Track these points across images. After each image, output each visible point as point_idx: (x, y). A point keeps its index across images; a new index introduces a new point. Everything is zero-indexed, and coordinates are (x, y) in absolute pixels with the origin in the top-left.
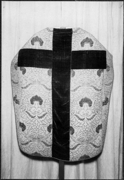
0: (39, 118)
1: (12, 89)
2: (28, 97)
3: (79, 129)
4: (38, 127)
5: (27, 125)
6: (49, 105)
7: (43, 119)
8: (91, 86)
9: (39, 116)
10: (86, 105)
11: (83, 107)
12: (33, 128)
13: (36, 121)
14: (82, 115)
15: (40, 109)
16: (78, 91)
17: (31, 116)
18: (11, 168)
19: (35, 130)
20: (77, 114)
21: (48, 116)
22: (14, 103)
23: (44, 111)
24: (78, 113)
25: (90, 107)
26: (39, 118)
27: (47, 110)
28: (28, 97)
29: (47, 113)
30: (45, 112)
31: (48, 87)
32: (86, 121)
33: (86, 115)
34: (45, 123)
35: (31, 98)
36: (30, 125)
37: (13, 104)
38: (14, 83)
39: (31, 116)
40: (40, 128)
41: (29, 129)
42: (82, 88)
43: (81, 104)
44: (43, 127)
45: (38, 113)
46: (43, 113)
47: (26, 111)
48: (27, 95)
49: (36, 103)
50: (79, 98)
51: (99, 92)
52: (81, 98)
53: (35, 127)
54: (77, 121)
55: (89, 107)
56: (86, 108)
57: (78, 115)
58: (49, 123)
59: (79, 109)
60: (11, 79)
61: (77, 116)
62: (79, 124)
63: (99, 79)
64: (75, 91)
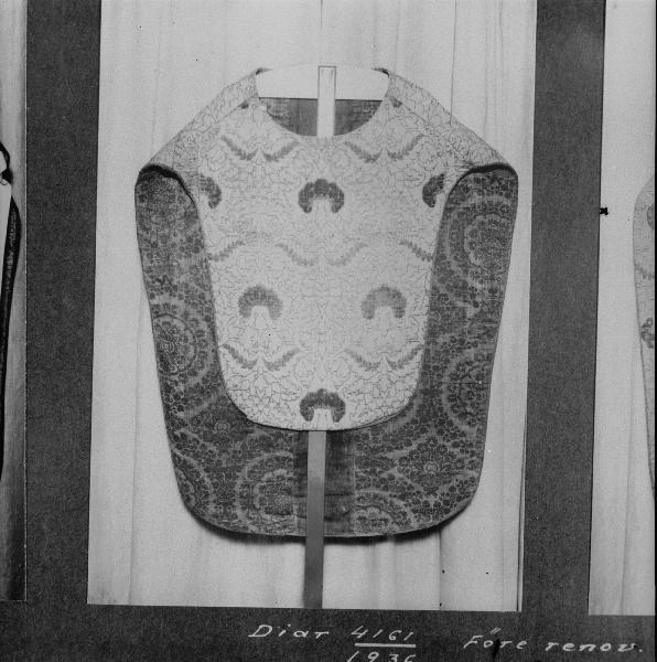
0: (271, 366)
1: (637, 296)
3: (362, 403)
5: (352, 397)
7: (283, 371)
8: (402, 243)
9: (268, 360)
10: (384, 312)
11: (374, 322)
17: (241, 360)
18: (624, 576)
22: (641, 347)
24: (359, 344)
26: (271, 366)
30: (290, 348)
31: (424, 247)
34: (292, 389)
35: (240, 294)
36: (361, 396)
37: (639, 350)
39: (241, 360)
44: (283, 402)
49: (260, 310)
51: (308, 269)
55: (395, 321)
57: (361, 352)
60: (634, 261)
62: (361, 382)
64: (344, 264)
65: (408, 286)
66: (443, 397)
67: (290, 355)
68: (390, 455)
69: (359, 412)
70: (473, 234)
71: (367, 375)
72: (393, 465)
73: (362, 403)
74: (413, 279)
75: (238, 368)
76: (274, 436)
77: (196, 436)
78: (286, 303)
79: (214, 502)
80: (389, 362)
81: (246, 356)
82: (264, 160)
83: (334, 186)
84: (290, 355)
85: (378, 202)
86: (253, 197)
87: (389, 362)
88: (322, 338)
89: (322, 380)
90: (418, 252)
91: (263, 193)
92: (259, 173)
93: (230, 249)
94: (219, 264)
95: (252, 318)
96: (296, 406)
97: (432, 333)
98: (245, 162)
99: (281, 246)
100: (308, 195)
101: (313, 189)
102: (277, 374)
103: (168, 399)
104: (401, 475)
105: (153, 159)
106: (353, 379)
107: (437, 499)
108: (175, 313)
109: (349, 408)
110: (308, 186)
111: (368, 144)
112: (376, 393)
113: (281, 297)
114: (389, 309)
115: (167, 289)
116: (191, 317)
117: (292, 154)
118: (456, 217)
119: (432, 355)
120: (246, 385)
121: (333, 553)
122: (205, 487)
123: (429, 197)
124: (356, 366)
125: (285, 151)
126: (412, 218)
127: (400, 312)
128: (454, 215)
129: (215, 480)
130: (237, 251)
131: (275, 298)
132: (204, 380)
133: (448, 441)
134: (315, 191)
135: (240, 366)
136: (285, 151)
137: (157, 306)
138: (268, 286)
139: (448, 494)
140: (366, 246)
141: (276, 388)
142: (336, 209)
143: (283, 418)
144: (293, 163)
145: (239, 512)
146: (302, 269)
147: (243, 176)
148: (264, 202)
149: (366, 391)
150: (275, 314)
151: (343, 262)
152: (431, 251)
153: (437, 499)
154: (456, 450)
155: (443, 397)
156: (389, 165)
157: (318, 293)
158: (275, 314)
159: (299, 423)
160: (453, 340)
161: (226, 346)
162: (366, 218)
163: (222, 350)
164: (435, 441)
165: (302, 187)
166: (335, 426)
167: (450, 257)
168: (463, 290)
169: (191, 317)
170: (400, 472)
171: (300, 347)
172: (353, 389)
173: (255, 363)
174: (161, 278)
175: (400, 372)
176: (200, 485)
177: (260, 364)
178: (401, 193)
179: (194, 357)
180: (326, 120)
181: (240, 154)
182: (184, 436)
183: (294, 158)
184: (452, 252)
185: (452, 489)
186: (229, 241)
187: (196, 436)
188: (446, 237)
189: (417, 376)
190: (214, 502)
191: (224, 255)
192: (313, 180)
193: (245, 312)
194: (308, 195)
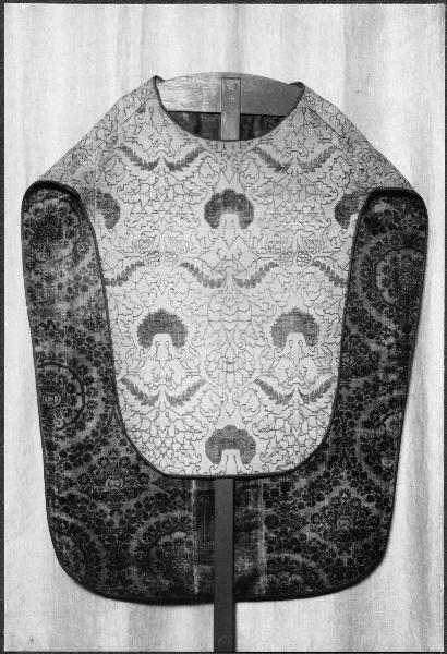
0: (174, 401)
2: (130, 318)
3: (273, 441)
4: (168, 443)
6: (212, 348)
9: (171, 394)
10: (296, 338)
12: (284, 444)
13: (163, 415)
14: (147, 380)
15: (175, 364)
16: (267, 286)
19: (291, 450)
20: (264, 379)
21: (209, 393)
23: (190, 374)
24: (269, 374)
25: (312, 348)
26: (174, 401)
27: (202, 367)
28: (130, 318)
29: (202, 382)
30: (196, 379)
31: (338, 272)
32: (296, 406)
33: (163, 381)
34: (198, 427)
35: (139, 321)
38: (30, 265)
40: (176, 446)
41: (270, 451)
42: (149, 271)
43: (279, 334)
44: (187, 443)
45: (169, 384)
46: (190, 382)
47: (255, 376)
48: (126, 311)
49: (163, 339)
50: (137, 312)
51: (216, 289)
52: (146, 313)
53: (158, 442)
54: (263, 408)
55: (306, 349)
56: (163, 355)
57: (270, 382)
58: (211, 426)
59: (271, 355)
61: (264, 387)
63: (211, 236)
64: (254, 286)
66: (357, 447)
67: (196, 387)
68: (302, 513)
70: (385, 269)
71: (277, 177)
72: (305, 524)
73: (273, 441)
74: (326, 305)
75: (138, 405)
76: (175, 486)
77: (86, 496)
78: (191, 330)
79: (107, 566)
80: (301, 395)
81: (145, 390)
82: (167, 169)
83: (242, 197)
84: (196, 387)
85: (289, 217)
86: (156, 212)
87: (301, 395)
88: (230, 368)
89: (230, 416)
91: (166, 206)
92: (162, 183)
93: (129, 270)
95: (153, 348)
96: (201, 447)
97: (345, 375)
98: (146, 172)
99: (185, 265)
100: (212, 211)
101: (220, 200)
102: (180, 410)
103: (51, 459)
104: (314, 535)
105: (46, 175)
107: (351, 556)
108: (62, 361)
109: (260, 446)
110: (216, 197)
111: (278, 151)
112: (288, 427)
113: (186, 322)
114: (300, 336)
115: (52, 335)
116: (79, 365)
117: (198, 161)
118: (368, 252)
119: (345, 400)
120: (146, 424)
121: (243, 609)
122: (96, 551)
123: (341, 214)
124: (266, 398)
125: (190, 158)
127: (311, 338)
128: (366, 250)
129: (106, 542)
130: (136, 275)
131: (180, 324)
132: (94, 433)
133: (362, 494)
134: (226, 202)
135: (140, 402)
136: (190, 158)
137: (42, 354)
138: (170, 310)
139: (362, 552)
140: (277, 265)
141: (180, 425)
142: (246, 223)
143: (187, 461)
144: (198, 171)
145: (134, 577)
146: (209, 290)
147: (145, 188)
148: (168, 216)
150: (179, 342)
151: (253, 282)
152: (345, 276)
153: (351, 556)
154: (371, 505)
155: (357, 447)
156: (302, 408)
157: (225, 317)
158: (179, 342)
159: (206, 468)
160: (366, 384)
161: (123, 380)
163: (120, 385)
164: (349, 494)
165: (208, 199)
166: (245, 470)
167: (362, 296)
168: (373, 329)
169: (79, 365)
170: (313, 531)
172: (263, 425)
173: (156, 398)
174: (46, 322)
175: (312, 406)
176: (92, 548)
177: (162, 398)
179: (82, 409)
180: (230, 127)
181: (140, 164)
182: (72, 497)
183: (199, 167)
184: (364, 290)
185: (366, 546)
186: (128, 263)
187: (86, 496)
188: (357, 274)
189: (330, 411)
190: (107, 566)
191: (121, 280)
192: (220, 190)
194: (212, 211)
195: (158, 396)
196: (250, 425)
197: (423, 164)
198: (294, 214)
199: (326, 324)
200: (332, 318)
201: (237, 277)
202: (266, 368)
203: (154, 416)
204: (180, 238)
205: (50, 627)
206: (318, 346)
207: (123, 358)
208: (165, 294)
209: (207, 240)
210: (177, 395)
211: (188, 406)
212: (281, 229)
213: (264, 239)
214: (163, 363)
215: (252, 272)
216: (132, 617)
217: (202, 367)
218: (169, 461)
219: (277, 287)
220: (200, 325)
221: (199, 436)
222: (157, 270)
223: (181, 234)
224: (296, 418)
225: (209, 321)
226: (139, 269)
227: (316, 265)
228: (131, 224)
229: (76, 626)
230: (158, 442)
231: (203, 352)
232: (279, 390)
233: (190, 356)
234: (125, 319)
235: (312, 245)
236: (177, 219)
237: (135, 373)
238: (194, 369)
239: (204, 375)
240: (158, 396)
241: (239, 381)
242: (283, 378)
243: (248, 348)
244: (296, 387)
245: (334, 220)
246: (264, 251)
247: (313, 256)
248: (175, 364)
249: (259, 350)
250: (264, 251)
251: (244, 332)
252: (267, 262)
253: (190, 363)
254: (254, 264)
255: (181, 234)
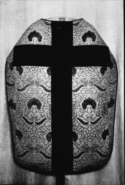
0: (37, 124)
6: (48, 110)
9: (92, 121)
13: (34, 127)
14: (85, 118)
21: (48, 122)
23: (42, 117)
24: (82, 116)
26: (37, 124)
27: (46, 115)
28: (80, 101)
29: (46, 119)
30: (44, 118)
31: (47, 88)
32: (90, 125)
33: (90, 118)
36: (82, 133)
40: (38, 136)
45: (91, 119)
46: (42, 119)
47: (23, 116)
50: (27, 99)
54: (25, 125)
62: (82, 129)
65: (42, 99)
69: (82, 138)
71: (84, 126)
80: (91, 122)
86: (33, 71)
87: (91, 122)
90: (46, 90)
94: (76, 93)
95: (87, 109)
106: (80, 127)
126: (44, 78)
127: (94, 107)
130: (27, 88)
141: (39, 130)
149: (84, 131)
162: (29, 77)
171: (102, 116)
173: (33, 123)
178: (40, 70)
186: (79, 85)
191: (76, 90)
193: (84, 107)
195: (88, 122)
196: (21, 129)
197: (118, 55)
198: (88, 71)
199: (44, 103)
200: (100, 100)
201: (18, 88)
202: (81, 115)
203: (87, 128)
204: (94, 78)
205: (13, 177)
206: (96, 109)
207: (78, 112)
208: (35, 94)
209: (48, 79)
210: (94, 122)
211: (41, 125)
212: (84, 75)
213: (79, 79)
214: (34, 113)
215: (22, 87)
216: (35, 175)
217: (46, 115)
218: (92, 140)
219: (83, 92)
220: (100, 102)
221: (45, 134)
222: (33, 87)
223: (40, 77)
224: (90, 129)
225: (48, 101)
226: (82, 87)
227: (41, 86)
228: (79, 74)
229: (20, 177)
230: (88, 135)
231: (46, 110)
232: (84, 121)
233: (42, 112)
234: (78, 101)
235: (94, 80)
236: (93, 72)
237: (27, 116)
238: (43, 115)
239: (47, 117)
240: (88, 122)
241: (18, 117)
242: (30, 117)
243: (21, 108)
244: (89, 120)
245: (100, 73)
246: (79, 82)
247: (40, 83)
248: (93, 113)
249: (78, 110)
250: (79, 82)
251: (20, 104)
252: (81, 85)
253: (42, 114)
254: (23, 85)
255: (40, 77)
